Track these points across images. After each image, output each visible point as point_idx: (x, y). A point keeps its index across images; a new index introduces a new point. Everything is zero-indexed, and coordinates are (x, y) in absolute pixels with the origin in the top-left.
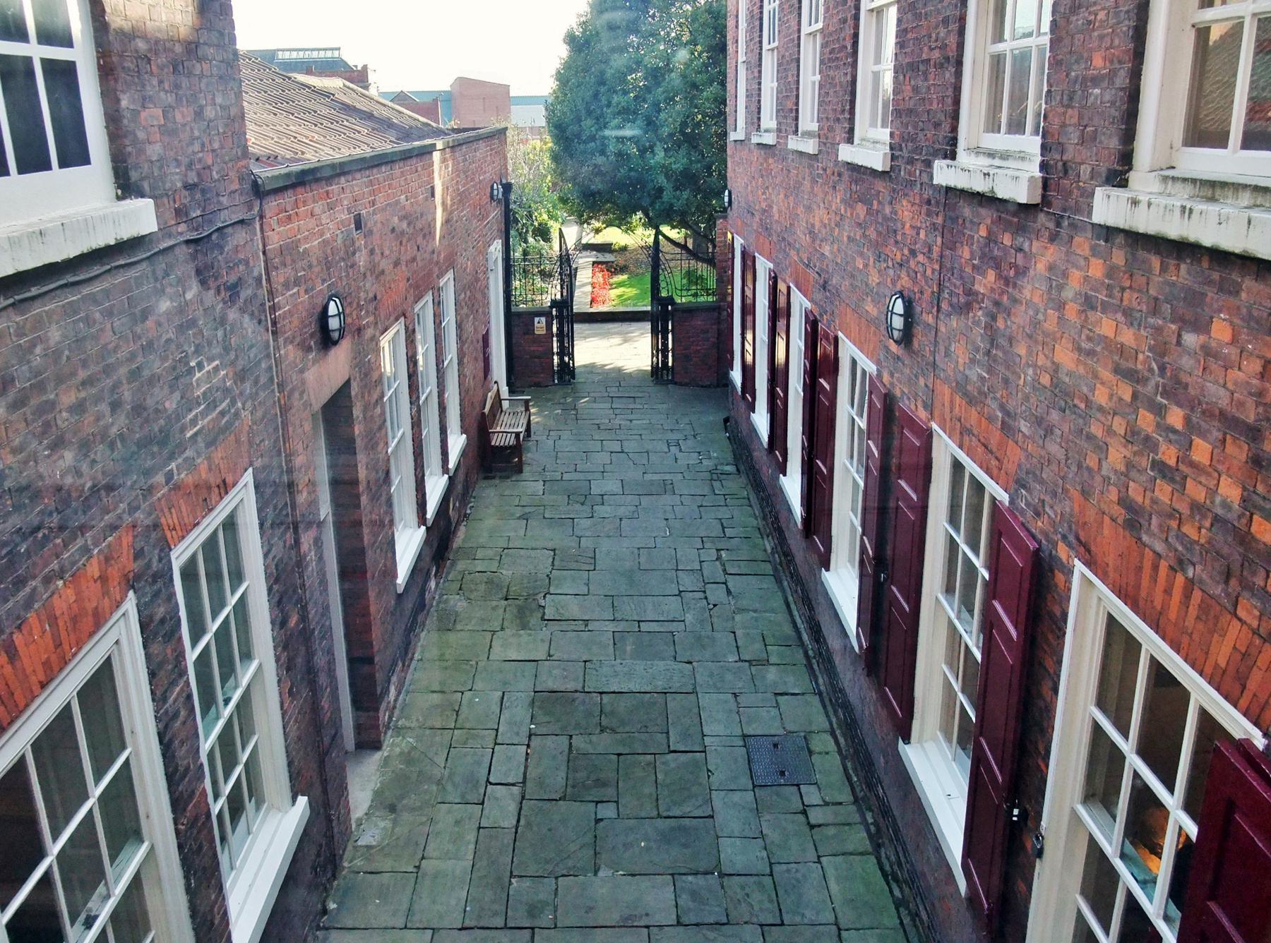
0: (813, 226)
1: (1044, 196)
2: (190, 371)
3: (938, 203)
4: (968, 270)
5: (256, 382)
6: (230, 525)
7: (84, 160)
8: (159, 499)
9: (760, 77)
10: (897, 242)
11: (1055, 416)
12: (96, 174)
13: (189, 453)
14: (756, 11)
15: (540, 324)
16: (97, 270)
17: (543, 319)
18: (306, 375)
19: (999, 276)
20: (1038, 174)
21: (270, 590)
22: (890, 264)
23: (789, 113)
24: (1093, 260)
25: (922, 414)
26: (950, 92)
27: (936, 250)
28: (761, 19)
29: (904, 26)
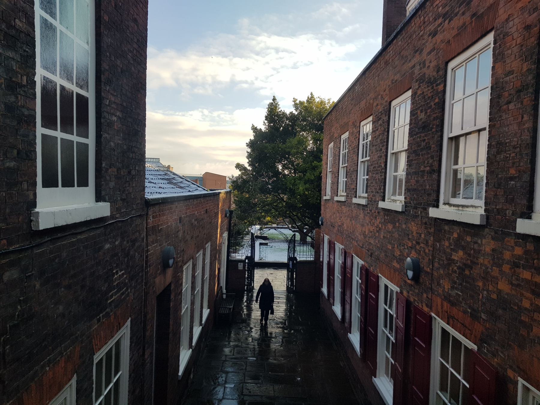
0: (365, 232)
1: (487, 222)
2: (113, 275)
3: (430, 224)
4: (448, 250)
5: (137, 281)
6: (118, 344)
7: (86, 185)
8: (93, 330)
9: (338, 176)
10: (409, 239)
11: (500, 312)
12: (90, 191)
13: (107, 310)
14: (337, 153)
15: (240, 266)
16: (84, 229)
17: (242, 264)
18: (156, 279)
19: (465, 253)
20: (483, 213)
21: (130, 376)
22: (406, 247)
23: (352, 191)
24: (516, 248)
25: (426, 309)
26: (436, 182)
27: (430, 242)
28: (339, 156)
29: (411, 158)
